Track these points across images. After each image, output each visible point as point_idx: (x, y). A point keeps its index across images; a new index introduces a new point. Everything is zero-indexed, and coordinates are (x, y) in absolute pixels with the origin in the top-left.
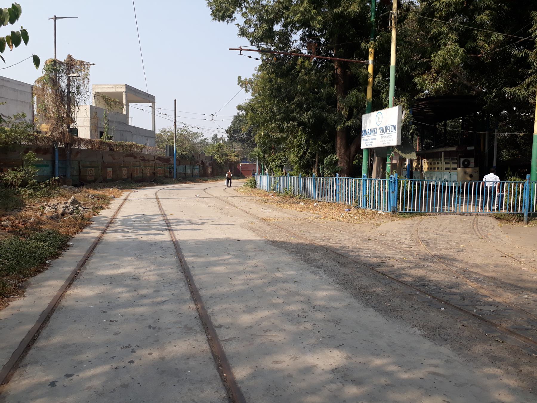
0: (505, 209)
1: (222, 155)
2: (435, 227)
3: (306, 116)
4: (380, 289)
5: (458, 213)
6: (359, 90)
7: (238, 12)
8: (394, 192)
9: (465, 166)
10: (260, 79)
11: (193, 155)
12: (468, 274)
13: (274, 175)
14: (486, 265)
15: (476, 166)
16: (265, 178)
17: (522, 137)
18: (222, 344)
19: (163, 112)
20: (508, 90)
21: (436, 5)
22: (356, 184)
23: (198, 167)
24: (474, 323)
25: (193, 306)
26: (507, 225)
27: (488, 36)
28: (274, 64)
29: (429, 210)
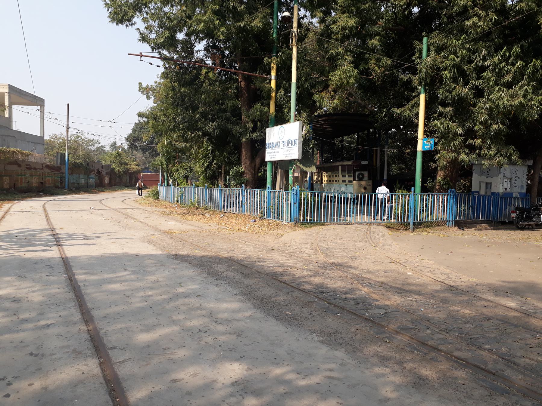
0: (394, 219)
1: (121, 164)
3: (211, 127)
4: (282, 298)
5: (353, 222)
6: (262, 104)
7: (138, 16)
8: (296, 203)
9: (360, 179)
10: (162, 87)
11: (88, 164)
12: (361, 280)
13: (178, 185)
14: (378, 271)
15: (369, 179)
16: (168, 189)
18: (116, 366)
19: (53, 116)
20: (396, 110)
21: (333, 27)
22: (261, 196)
23: (93, 176)
25: (84, 327)
26: (396, 234)
27: (378, 60)
28: (177, 73)
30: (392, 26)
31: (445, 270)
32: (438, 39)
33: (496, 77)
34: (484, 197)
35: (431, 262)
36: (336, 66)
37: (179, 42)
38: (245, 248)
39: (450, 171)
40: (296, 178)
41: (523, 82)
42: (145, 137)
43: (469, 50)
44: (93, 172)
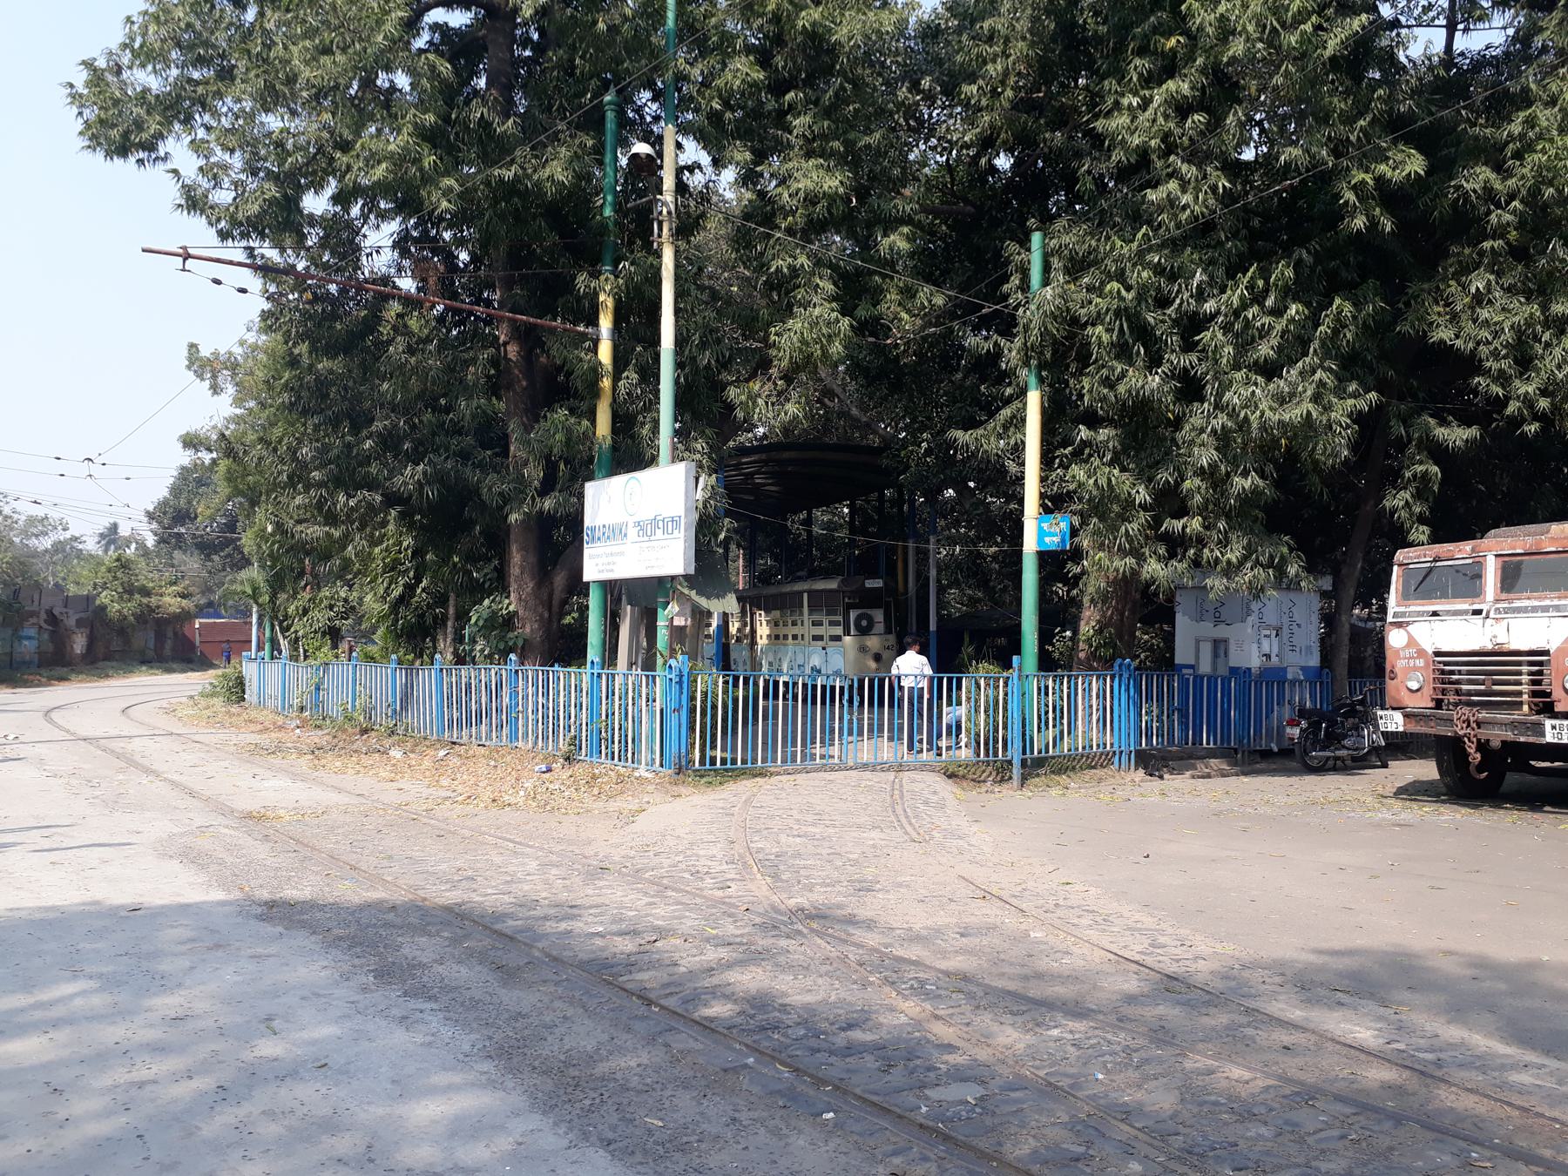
2: (794, 812)
3: (409, 477)
4: (632, 1061)
5: (851, 763)
6: (572, 411)
8: (677, 710)
9: (864, 631)
10: (262, 357)
11: (16, 593)
12: (892, 969)
13: (306, 657)
14: (938, 931)
15: (888, 631)
16: (274, 670)
17: (995, 557)
20: (961, 436)
22: (570, 685)
23: (32, 632)
24: (925, 1159)
27: (909, 293)
28: (304, 313)
29: (774, 760)
30: (942, 203)
31: (1137, 916)
32: (1071, 237)
33: (1236, 346)
34: (1212, 679)
35: (1093, 890)
36: (790, 306)
37: (312, 220)
38: (511, 869)
39: (1116, 608)
40: (677, 633)
41: (1307, 360)
42: (209, 510)
43: (1158, 270)
44: (34, 620)
